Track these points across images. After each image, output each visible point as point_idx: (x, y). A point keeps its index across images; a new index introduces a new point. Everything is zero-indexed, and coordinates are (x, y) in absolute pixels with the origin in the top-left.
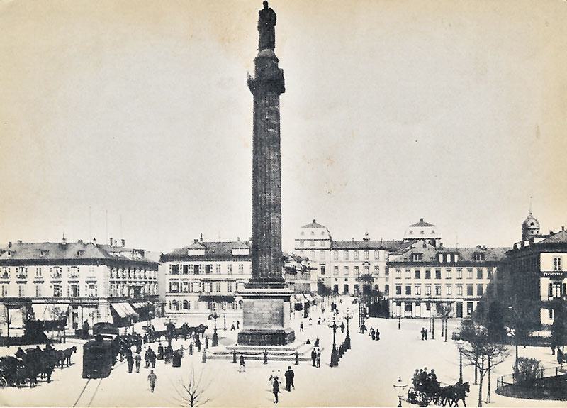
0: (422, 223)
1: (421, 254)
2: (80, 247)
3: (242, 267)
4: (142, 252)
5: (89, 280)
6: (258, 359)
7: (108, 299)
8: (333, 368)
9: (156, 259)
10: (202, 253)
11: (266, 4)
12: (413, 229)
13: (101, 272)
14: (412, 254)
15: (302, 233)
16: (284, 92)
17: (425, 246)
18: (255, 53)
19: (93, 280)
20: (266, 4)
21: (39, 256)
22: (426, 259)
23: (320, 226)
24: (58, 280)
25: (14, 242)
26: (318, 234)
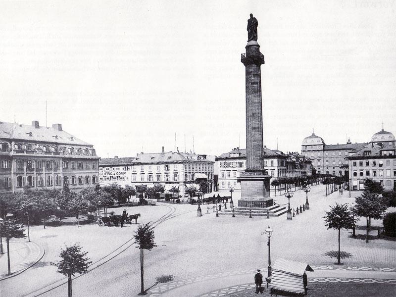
0: (383, 132)
1: (370, 151)
2: (170, 155)
3: (272, 162)
4: (205, 156)
5: (175, 172)
6: (246, 215)
7: (184, 182)
8: (141, 215)
9: (213, 160)
10: (237, 155)
11: (251, 15)
12: (377, 136)
13: (180, 168)
14: (364, 152)
15: (30, 133)
16: (264, 63)
17: (373, 146)
18: (246, 43)
19: (176, 172)
20: (251, 15)
21: (150, 161)
22: (373, 154)
23: (317, 137)
24: (168, 172)
25: (139, 153)
26: (316, 141)
